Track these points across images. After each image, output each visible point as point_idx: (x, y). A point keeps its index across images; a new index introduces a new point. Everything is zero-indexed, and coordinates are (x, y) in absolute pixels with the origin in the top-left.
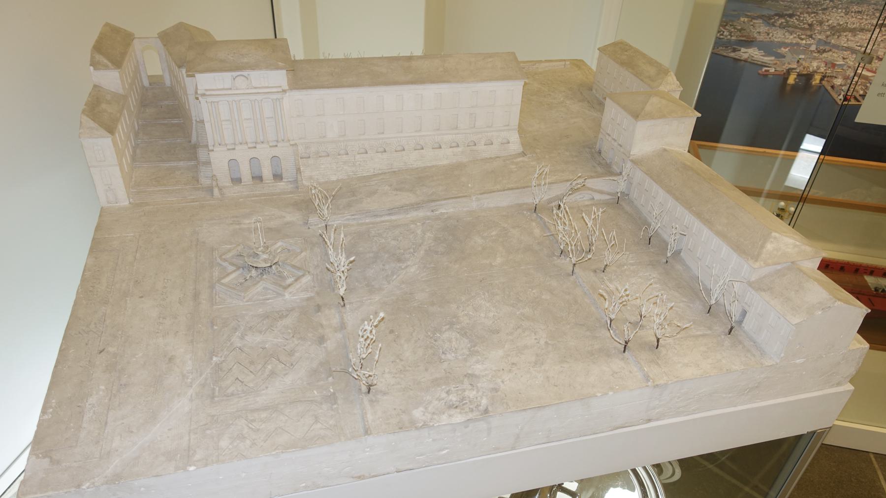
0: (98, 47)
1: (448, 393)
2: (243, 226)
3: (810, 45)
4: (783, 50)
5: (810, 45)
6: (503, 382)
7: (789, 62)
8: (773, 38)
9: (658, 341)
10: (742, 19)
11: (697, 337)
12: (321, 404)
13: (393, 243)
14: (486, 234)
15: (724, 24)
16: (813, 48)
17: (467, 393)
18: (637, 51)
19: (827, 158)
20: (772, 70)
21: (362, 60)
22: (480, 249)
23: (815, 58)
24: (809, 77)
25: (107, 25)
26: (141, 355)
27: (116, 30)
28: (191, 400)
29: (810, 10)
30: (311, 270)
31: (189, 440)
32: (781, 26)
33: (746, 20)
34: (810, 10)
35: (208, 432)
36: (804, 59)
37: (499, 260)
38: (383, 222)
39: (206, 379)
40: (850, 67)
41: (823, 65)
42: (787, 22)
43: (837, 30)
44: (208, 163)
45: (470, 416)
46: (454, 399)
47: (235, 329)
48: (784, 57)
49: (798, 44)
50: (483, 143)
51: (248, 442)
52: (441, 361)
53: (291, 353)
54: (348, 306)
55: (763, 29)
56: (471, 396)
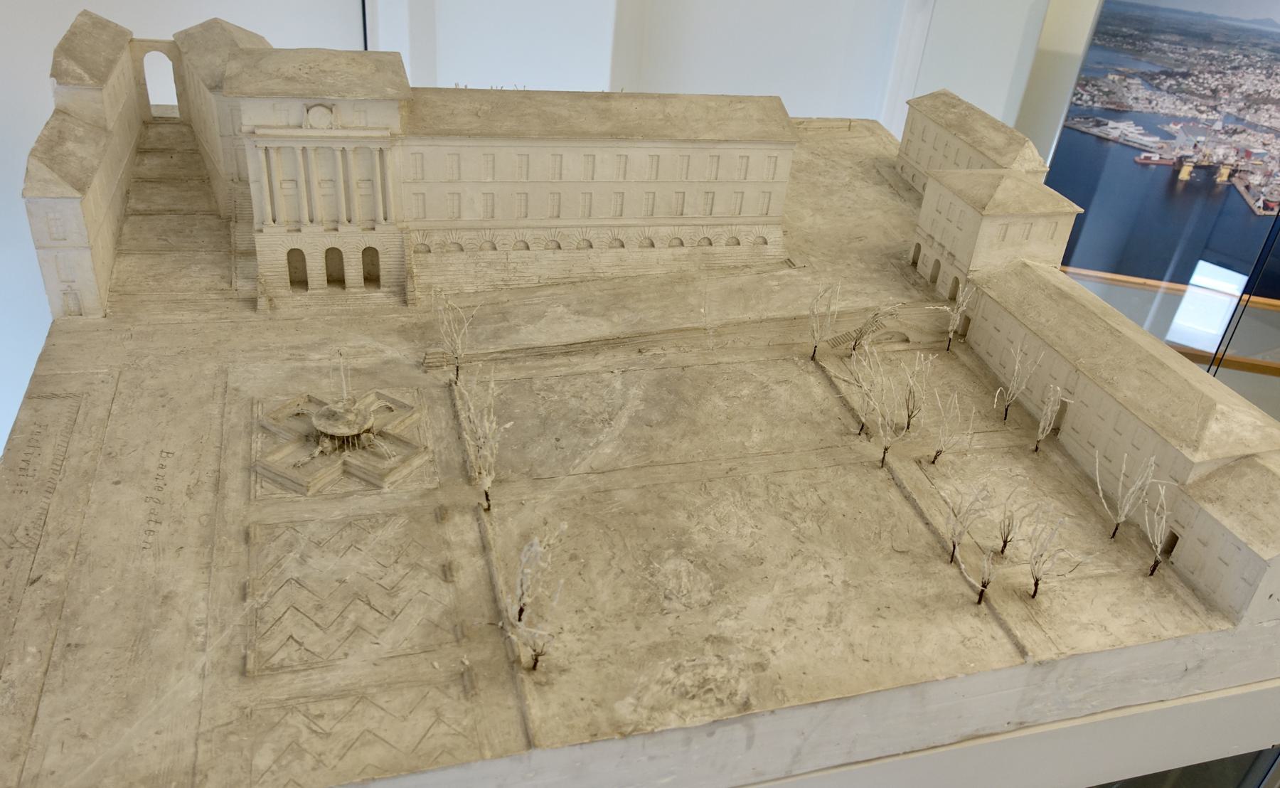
0: (67, 48)
1: (677, 669)
2: (308, 364)
3: (1213, 122)
4: (1173, 128)
5: (1213, 122)
6: (773, 652)
7: (1182, 146)
8: (1157, 109)
9: (1036, 584)
10: (1111, 77)
11: (1097, 578)
12: (447, 687)
13: (574, 403)
14: (731, 393)
15: (1083, 82)
16: (1218, 126)
17: (711, 672)
18: (970, 108)
19: (1253, 298)
20: (1156, 158)
21: (527, 95)
22: (722, 418)
23: (1220, 142)
24: (1211, 170)
25: (85, 13)
26: (109, 589)
27: (100, 24)
28: (203, 676)
29: (1213, 68)
30: (430, 445)
31: (196, 753)
32: (1170, 91)
33: (1117, 77)
34: (1213, 68)
35: (233, 739)
36: (1204, 143)
37: (756, 437)
38: (556, 366)
39: (232, 638)
40: (1273, 158)
41: (1233, 153)
42: (1179, 84)
43: (1254, 101)
44: (251, 253)
45: (719, 712)
46: (689, 683)
47: (290, 546)
48: (1173, 137)
49: (1195, 119)
50: (724, 242)
51: (309, 760)
52: (664, 612)
53: (392, 591)
54: (494, 510)
55: (1144, 93)
56: (718, 677)
